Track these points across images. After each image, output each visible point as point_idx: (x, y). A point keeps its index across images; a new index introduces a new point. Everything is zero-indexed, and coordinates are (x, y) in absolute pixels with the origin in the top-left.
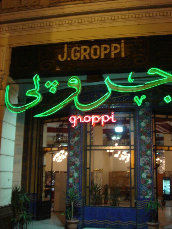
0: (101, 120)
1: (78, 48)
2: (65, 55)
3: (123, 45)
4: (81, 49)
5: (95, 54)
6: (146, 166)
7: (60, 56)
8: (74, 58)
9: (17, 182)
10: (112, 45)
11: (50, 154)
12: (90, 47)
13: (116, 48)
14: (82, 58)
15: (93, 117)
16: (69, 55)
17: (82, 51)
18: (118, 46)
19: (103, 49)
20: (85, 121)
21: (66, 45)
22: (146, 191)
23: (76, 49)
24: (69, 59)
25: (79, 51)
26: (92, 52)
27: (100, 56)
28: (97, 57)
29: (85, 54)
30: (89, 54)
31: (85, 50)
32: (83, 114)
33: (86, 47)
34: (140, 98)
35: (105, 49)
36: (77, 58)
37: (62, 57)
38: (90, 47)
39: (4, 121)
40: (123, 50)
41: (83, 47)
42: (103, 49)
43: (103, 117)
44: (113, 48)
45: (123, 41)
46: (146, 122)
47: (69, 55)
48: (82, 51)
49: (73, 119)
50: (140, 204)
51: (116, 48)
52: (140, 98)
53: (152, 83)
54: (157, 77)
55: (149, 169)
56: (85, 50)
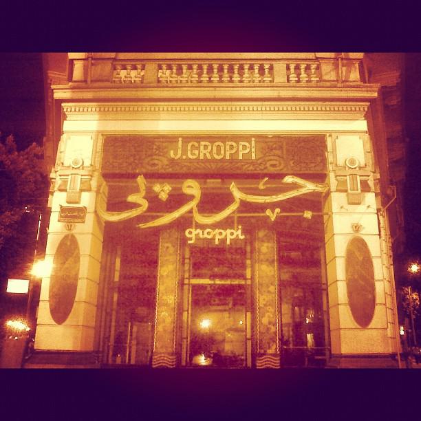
0: (226, 236)
1: (196, 144)
2: (180, 152)
3: (253, 143)
4: (199, 145)
5: (218, 153)
6: (268, 308)
7: (172, 152)
8: (191, 157)
9: (288, 68)
10: (240, 143)
11: (328, 270)
12: (212, 143)
13: (245, 147)
14: (202, 157)
15: (217, 231)
16: (184, 151)
17: (202, 148)
18: (247, 144)
19: (228, 147)
20: (206, 236)
21: (180, 139)
22: (268, 343)
23: (193, 145)
24: (184, 157)
25: (198, 148)
26: (215, 151)
27: (225, 156)
28: (220, 157)
29: (204, 152)
30: (211, 152)
31: (206, 147)
32: (203, 227)
33: (207, 143)
34: (273, 212)
35: (232, 147)
36: (195, 157)
37: (176, 154)
38: (212, 143)
39: (96, 261)
40: (253, 150)
41: (203, 143)
42: (228, 147)
43: (229, 231)
44: (241, 147)
45: (253, 139)
46: (268, 247)
47: (184, 151)
48: (202, 148)
49: (190, 233)
50: (260, 365)
51: (245, 147)
52: (273, 212)
53: (245, 217)
54: (294, 186)
55: (271, 312)
56: (206, 147)
